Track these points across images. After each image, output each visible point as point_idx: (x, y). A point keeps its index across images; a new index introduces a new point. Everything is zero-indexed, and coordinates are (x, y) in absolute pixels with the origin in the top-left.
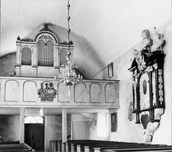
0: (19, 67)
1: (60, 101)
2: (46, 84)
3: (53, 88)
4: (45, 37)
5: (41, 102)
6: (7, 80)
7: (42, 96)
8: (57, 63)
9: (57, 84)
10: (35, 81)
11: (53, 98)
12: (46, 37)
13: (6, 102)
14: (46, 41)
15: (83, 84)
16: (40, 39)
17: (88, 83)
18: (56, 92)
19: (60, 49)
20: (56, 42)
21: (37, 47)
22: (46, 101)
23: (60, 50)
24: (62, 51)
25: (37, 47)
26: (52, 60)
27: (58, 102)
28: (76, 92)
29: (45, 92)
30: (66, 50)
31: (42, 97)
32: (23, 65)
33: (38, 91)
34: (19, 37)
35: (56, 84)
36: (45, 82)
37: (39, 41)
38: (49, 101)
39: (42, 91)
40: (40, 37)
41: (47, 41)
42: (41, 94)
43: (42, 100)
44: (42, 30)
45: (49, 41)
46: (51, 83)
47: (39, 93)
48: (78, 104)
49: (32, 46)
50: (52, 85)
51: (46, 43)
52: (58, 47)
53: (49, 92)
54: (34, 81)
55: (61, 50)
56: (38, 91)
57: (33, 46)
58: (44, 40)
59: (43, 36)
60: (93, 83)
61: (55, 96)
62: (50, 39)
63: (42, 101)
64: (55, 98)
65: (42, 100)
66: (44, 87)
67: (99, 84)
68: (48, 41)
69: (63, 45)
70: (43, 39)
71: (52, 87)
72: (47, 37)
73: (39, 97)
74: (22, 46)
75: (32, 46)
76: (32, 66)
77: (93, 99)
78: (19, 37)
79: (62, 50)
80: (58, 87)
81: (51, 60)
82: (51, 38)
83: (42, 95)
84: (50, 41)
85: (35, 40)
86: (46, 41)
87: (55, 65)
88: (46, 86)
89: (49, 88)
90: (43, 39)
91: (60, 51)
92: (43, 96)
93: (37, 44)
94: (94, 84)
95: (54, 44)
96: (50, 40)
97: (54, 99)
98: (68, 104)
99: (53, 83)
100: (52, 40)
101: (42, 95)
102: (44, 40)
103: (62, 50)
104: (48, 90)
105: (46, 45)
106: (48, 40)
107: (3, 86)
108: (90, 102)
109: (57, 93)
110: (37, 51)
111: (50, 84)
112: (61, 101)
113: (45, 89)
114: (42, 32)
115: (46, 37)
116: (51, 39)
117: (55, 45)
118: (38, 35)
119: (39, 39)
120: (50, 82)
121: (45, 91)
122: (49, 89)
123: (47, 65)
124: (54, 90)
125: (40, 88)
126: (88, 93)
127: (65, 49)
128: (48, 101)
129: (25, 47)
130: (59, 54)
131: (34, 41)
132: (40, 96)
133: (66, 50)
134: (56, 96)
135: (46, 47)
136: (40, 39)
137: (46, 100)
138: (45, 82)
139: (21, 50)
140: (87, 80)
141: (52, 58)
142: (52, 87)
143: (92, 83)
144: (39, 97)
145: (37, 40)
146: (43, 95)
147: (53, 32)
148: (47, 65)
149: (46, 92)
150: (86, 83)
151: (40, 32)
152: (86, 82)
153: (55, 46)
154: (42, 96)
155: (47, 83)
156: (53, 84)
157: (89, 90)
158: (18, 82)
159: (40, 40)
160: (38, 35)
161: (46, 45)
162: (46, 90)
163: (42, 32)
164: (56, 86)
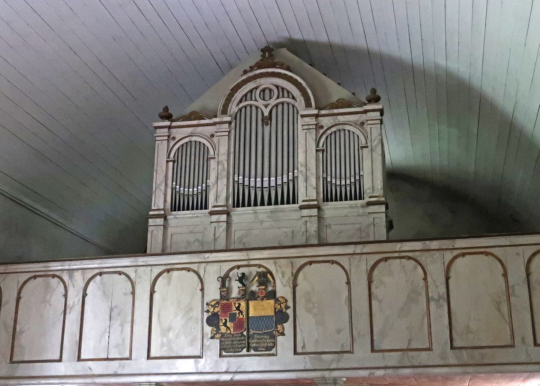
0: (162, 219)
1: (303, 347)
2: (242, 279)
3: (272, 295)
4: (264, 90)
5: (221, 356)
6: (157, 271)
7: (223, 329)
8: (309, 189)
9: (288, 274)
10: (196, 269)
11: (274, 337)
12: (267, 92)
13: (84, 363)
14: (266, 106)
15: (413, 263)
16: (241, 105)
17: (437, 254)
18: (287, 307)
19: (322, 127)
20: (308, 105)
21: (229, 136)
22: (244, 351)
23: (321, 131)
24: (333, 136)
25: (229, 136)
26: (357, 178)
27: (295, 353)
28: (380, 302)
29: (237, 312)
30: (347, 127)
31: (223, 335)
32: (241, 209)
33: (208, 311)
34: (166, 109)
35: (283, 274)
36: (238, 267)
37: (240, 110)
38: (256, 349)
39: (226, 308)
40: (246, 95)
41: (270, 107)
42: (221, 324)
43: (225, 350)
44: (252, 69)
45: (280, 107)
46: (261, 270)
47: (213, 320)
48: (393, 359)
49: (212, 136)
50: (268, 281)
51: (266, 114)
52: (312, 121)
53: (255, 310)
54: (194, 267)
55: (329, 132)
56: (208, 311)
57: (215, 134)
58: (260, 103)
59: (256, 88)
60: (464, 255)
61: (279, 327)
62: (291, 97)
63: (224, 353)
64: (283, 334)
65: (222, 349)
66: (235, 287)
67: (493, 255)
68: (277, 105)
69: (336, 111)
70: (256, 100)
71: (270, 289)
72: (270, 90)
73: (212, 338)
74: (174, 138)
75: (212, 136)
76: (210, 209)
77: (468, 329)
78: (166, 109)
79: (333, 129)
80: (295, 286)
81: (353, 180)
82: (288, 92)
83: (225, 324)
84: (283, 104)
85: (224, 112)
86: (266, 106)
87: (301, 196)
88: (241, 285)
89: (253, 293)
90: (256, 100)
91: (324, 137)
92: (228, 328)
93: (230, 123)
94: (467, 257)
95: (298, 113)
96: (281, 100)
97: (280, 339)
98: (347, 361)
99: (272, 269)
100: (293, 98)
101: (225, 324)
102: (260, 103)
103: (333, 129)
104: (251, 303)
105: (267, 120)
106: (273, 102)
107: (9, 296)
108: (452, 348)
109: (290, 312)
110: (232, 150)
111: (259, 274)
112: (309, 349)
113: (238, 299)
114: (251, 74)
115: (267, 92)
116: (288, 97)
117: (303, 116)
118: (234, 90)
119: (241, 101)
120: (260, 266)
121: (238, 308)
122: (256, 299)
123: (252, 203)
124: (277, 300)
125: (218, 297)
126: (437, 301)
127: (340, 127)
128: (252, 352)
129: (187, 143)
130: (317, 151)
131: (219, 113)
132: (218, 329)
133: (351, 129)
134: (288, 326)
135: (267, 129)
136: (241, 105)
137: (243, 348)
138: (238, 267)
139: (172, 155)
140: (428, 242)
141: (357, 172)
142: (266, 287)
143: (456, 253)
144: (212, 338)
145: (233, 108)
146: (228, 324)
147: (292, 68)
148: (252, 203)
149: (241, 312)
150: (424, 258)
151: (245, 77)
152: (426, 254)
153: (301, 121)
154: (223, 329)
155: (243, 274)
156: (274, 273)
157: (443, 290)
158: (132, 276)
159: (245, 107)
160: (234, 90)
161: (267, 120)
162: (243, 304)
163: (251, 74)
164: (285, 283)
